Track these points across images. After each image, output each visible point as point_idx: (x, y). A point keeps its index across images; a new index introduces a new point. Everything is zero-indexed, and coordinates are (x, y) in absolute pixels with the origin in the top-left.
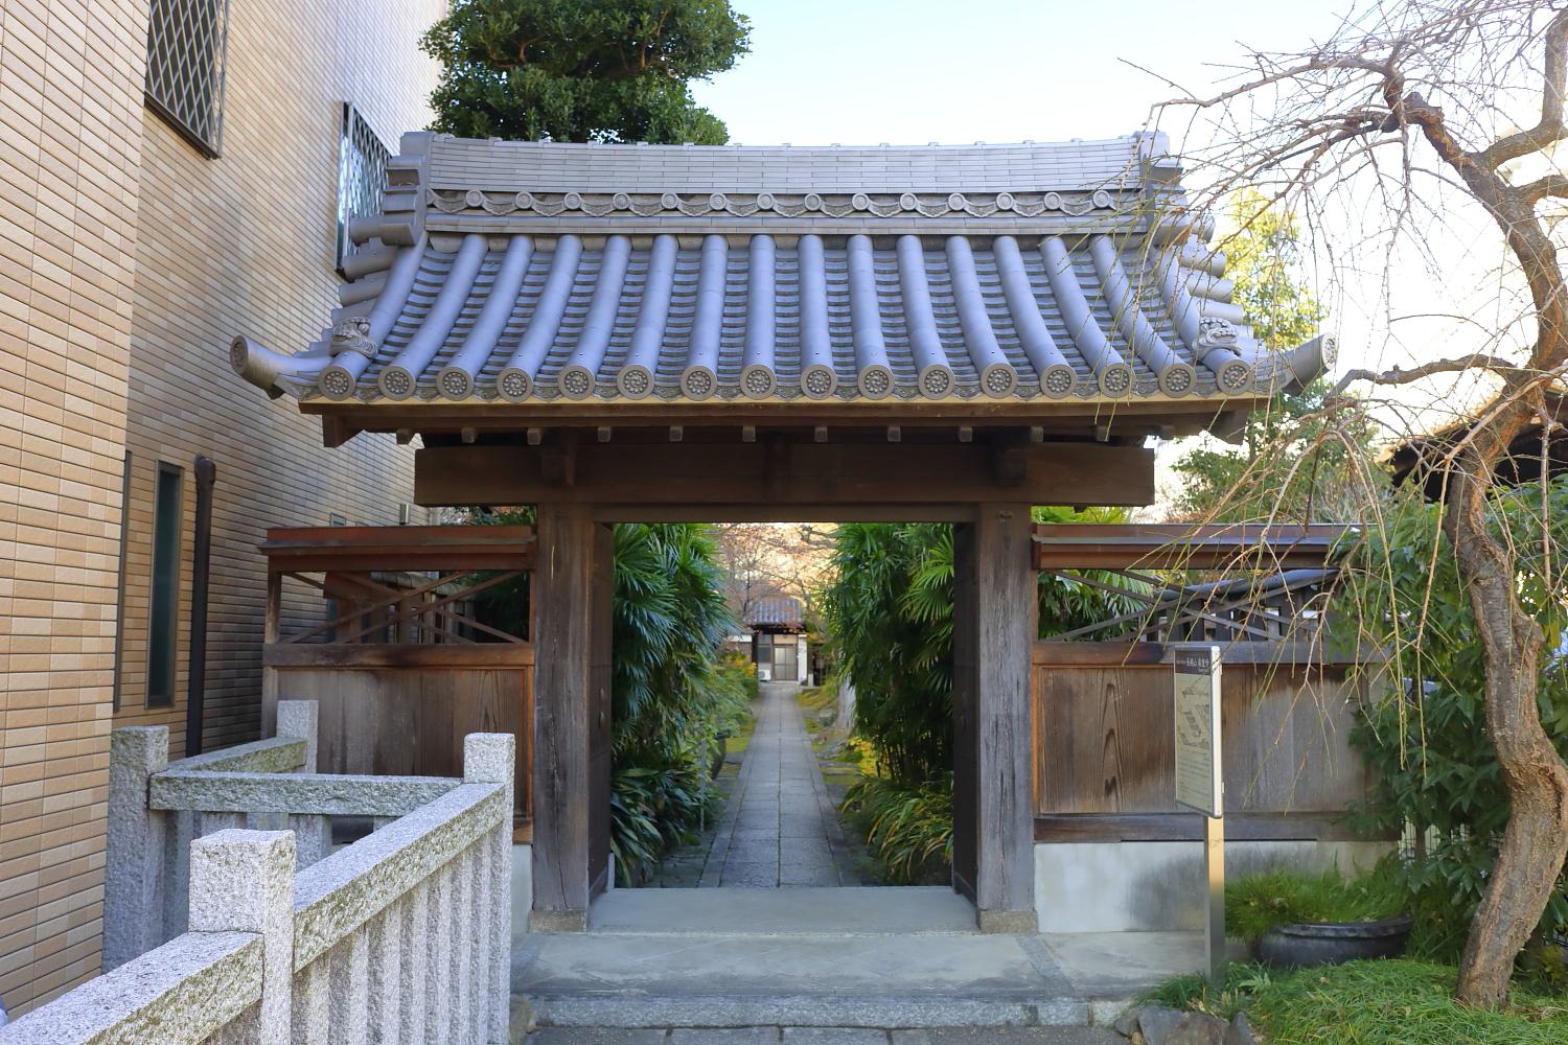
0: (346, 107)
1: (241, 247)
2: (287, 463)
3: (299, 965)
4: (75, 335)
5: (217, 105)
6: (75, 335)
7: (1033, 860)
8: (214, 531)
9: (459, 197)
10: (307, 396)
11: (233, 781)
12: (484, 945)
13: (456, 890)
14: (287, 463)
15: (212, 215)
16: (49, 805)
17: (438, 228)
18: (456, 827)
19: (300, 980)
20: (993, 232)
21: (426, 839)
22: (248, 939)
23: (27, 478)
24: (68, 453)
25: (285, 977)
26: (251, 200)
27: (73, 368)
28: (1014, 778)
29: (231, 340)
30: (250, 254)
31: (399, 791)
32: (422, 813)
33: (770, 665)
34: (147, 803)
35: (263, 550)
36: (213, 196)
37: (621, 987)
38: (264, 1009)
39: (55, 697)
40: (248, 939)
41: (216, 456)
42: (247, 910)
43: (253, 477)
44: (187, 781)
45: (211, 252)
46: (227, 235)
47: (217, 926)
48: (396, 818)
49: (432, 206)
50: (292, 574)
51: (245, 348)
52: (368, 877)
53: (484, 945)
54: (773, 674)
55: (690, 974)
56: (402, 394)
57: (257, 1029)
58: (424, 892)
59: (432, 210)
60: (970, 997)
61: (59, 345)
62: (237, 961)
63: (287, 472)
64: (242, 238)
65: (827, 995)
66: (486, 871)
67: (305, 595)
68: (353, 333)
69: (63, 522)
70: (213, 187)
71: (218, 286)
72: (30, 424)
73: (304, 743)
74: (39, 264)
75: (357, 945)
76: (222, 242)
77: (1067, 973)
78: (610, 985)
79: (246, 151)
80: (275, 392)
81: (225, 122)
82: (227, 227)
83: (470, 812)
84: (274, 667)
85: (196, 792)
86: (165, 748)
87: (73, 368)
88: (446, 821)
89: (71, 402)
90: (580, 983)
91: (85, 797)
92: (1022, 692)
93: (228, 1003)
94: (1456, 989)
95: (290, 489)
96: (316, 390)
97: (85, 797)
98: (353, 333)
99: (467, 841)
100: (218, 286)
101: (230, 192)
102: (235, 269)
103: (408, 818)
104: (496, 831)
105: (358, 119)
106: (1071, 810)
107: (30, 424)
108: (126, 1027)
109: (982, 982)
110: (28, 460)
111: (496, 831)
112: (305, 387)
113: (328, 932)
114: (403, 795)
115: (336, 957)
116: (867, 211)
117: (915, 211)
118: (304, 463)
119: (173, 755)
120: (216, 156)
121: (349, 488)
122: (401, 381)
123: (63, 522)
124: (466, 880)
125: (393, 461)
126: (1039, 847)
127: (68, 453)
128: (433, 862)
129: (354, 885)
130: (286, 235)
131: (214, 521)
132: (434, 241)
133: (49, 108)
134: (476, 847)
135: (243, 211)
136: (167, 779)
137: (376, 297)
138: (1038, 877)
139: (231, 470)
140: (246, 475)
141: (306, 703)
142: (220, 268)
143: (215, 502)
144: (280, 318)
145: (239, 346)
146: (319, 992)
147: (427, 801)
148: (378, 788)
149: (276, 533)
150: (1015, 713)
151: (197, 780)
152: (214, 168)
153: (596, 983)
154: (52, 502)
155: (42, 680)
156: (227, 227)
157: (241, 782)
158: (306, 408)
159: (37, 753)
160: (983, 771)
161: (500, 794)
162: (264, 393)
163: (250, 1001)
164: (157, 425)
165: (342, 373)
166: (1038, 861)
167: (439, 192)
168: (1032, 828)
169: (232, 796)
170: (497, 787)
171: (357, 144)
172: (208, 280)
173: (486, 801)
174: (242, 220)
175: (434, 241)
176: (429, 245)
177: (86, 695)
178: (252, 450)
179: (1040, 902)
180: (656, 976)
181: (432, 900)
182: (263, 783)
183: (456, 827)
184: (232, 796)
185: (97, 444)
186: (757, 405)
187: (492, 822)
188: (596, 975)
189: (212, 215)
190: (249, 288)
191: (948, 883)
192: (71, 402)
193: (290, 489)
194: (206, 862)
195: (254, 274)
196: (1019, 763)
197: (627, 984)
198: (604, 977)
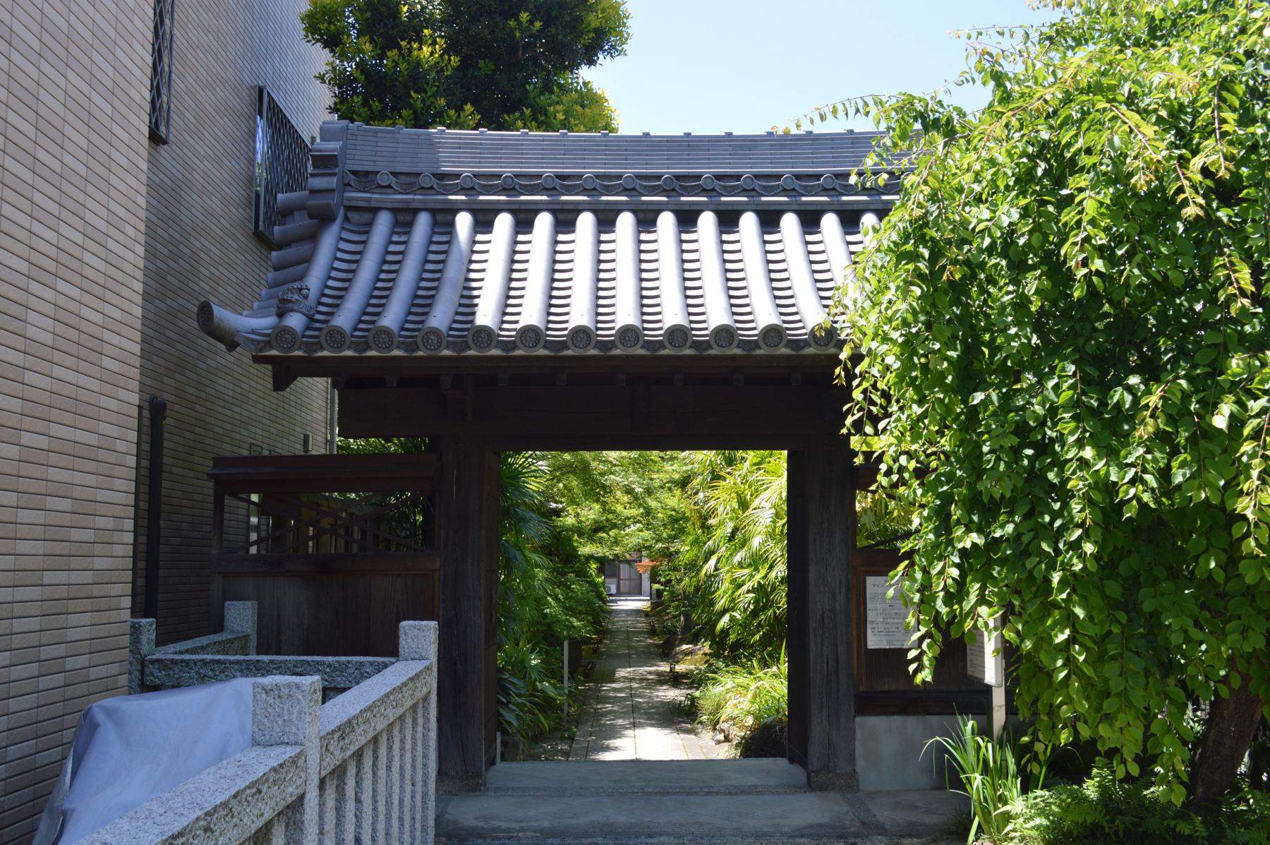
0: (261, 90)
1: (183, 217)
2: (217, 401)
3: (324, 773)
4: (109, 310)
5: (165, 99)
6: (109, 310)
7: (854, 731)
8: (165, 460)
9: (371, 177)
10: (261, 350)
11: (213, 661)
12: (419, 788)
13: (376, 758)
14: (217, 401)
15: (161, 192)
16: (95, 673)
17: (353, 203)
18: (404, 689)
19: (322, 783)
20: (819, 208)
21: (387, 695)
22: (298, 749)
23: (80, 421)
24: (104, 401)
25: (316, 781)
26: (189, 177)
27: (108, 336)
28: (837, 662)
29: (198, 303)
30: (189, 222)
31: (347, 667)
32: (367, 684)
33: (615, 580)
34: (142, 680)
35: (210, 476)
36: (162, 176)
37: (518, 831)
38: (306, 800)
39: (97, 590)
40: (298, 749)
41: (166, 396)
42: (294, 730)
43: (192, 413)
44: (174, 662)
45: (160, 223)
46: (172, 208)
47: (273, 741)
48: (344, 690)
49: (348, 184)
50: (235, 495)
51: (211, 311)
52: (356, 717)
53: (419, 788)
54: (618, 588)
55: (573, 821)
56: (340, 347)
57: (302, 814)
58: (385, 737)
59: (348, 188)
60: (802, 836)
61: (97, 317)
62: (294, 761)
63: (217, 408)
64: (183, 210)
65: (686, 835)
66: (420, 729)
67: (250, 516)
68: (296, 297)
69: (103, 455)
70: (162, 168)
71: (166, 252)
72: (83, 381)
73: (247, 636)
74: (87, 257)
75: (349, 768)
76: (167, 213)
77: (881, 819)
78: (508, 830)
79: (186, 135)
80: (232, 345)
81: (172, 114)
82: (172, 200)
83: (412, 679)
84: (219, 573)
85: (181, 671)
86: (153, 637)
87: (108, 336)
88: (399, 684)
89: (106, 362)
90: (483, 829)
91: (114, 669)
92: (843, 591)
93: (290, 790)
94: (321, 78)
95: (220, 423)
96: (268, 345)
97: (114, 669)
98: (296, 297)
99: (409, 703)
100: (166, 252)
101: (173, 170)
102: (178, 236)
103: (355, 691)
104: (426, 699)
105: (271, 100)
106: (886, 688)
107: (83, 381)
108: (248, 791)
109: (810, 826)
110: (81, 408)
111: (426, 699)
112: (258, 342)
113: (338, 756)
114: (350, 671)
115: (339, 772)
116: (713, 190)
117: (753, 190)
118: (230, 400)
119: (160, 642)
120: (165, 142)
121: (265, 421)
122: (337, 337)
123: (103, 455)
124: (383, 751)
125: (316, 397)
126: (858, 719)
127: (104, 401)
128: (392, 714)
129: (349, 722)
130: (215, 205)
131: (165, 452)
132: (350, 215)
133: (93, 137)
134: (414, 708)
135: (184, 187)
136: (158, 661)
137: (308, 260)
138: (858, 744)
139: (177, 408)
140: (186, 411)
141: (249, 603)
142: (166, 236)
143: (166, 435)
144: (89, 230)
145: (205, 311)
146: (331, 793)
147: (370, 676)
148: (330, 666)
149: (219, 461)
150: (838, 607)
151: (183, 661)
152: (162, 152)
153: (495, 829)
154: (93, 439)
155: (87, 577)
156: (172, 200)
157: (218, 662)
158: (257, 359)
159: (85, 633)
160: (812, 655)
161: (428, 668)
162: (222, 347)
163: (300, 791)
164: (172, 382)
165: (289, 330)
166: (858, 731)
167: (354, 173)
168: (852, 704)
169: (211, 674)
170: (426, 663)
171: (270, 124)
172: (159, 247)
173: (421, 672)
174: (183, 194)
175: (350, 215)
176: (346, 219)
177: (116, 589)
178: (193, 391)
179: (860, 765)
180: (546, 824)
181: (390, 739)
182: (237, 662)
183: (404, 689)
184: (211, 674)
185: (122, 394)
186: (627, 356)
187: (425, 690)
188: (496, 823)
189: (161, 192)
190: (188, 252)
191: (783, 756)
192: (106, 362)
193: (220, 423)
194: (264, 696)
195: (192, 240)
196: (841, 649)
197: (522, 829)
198: (504, 825)
